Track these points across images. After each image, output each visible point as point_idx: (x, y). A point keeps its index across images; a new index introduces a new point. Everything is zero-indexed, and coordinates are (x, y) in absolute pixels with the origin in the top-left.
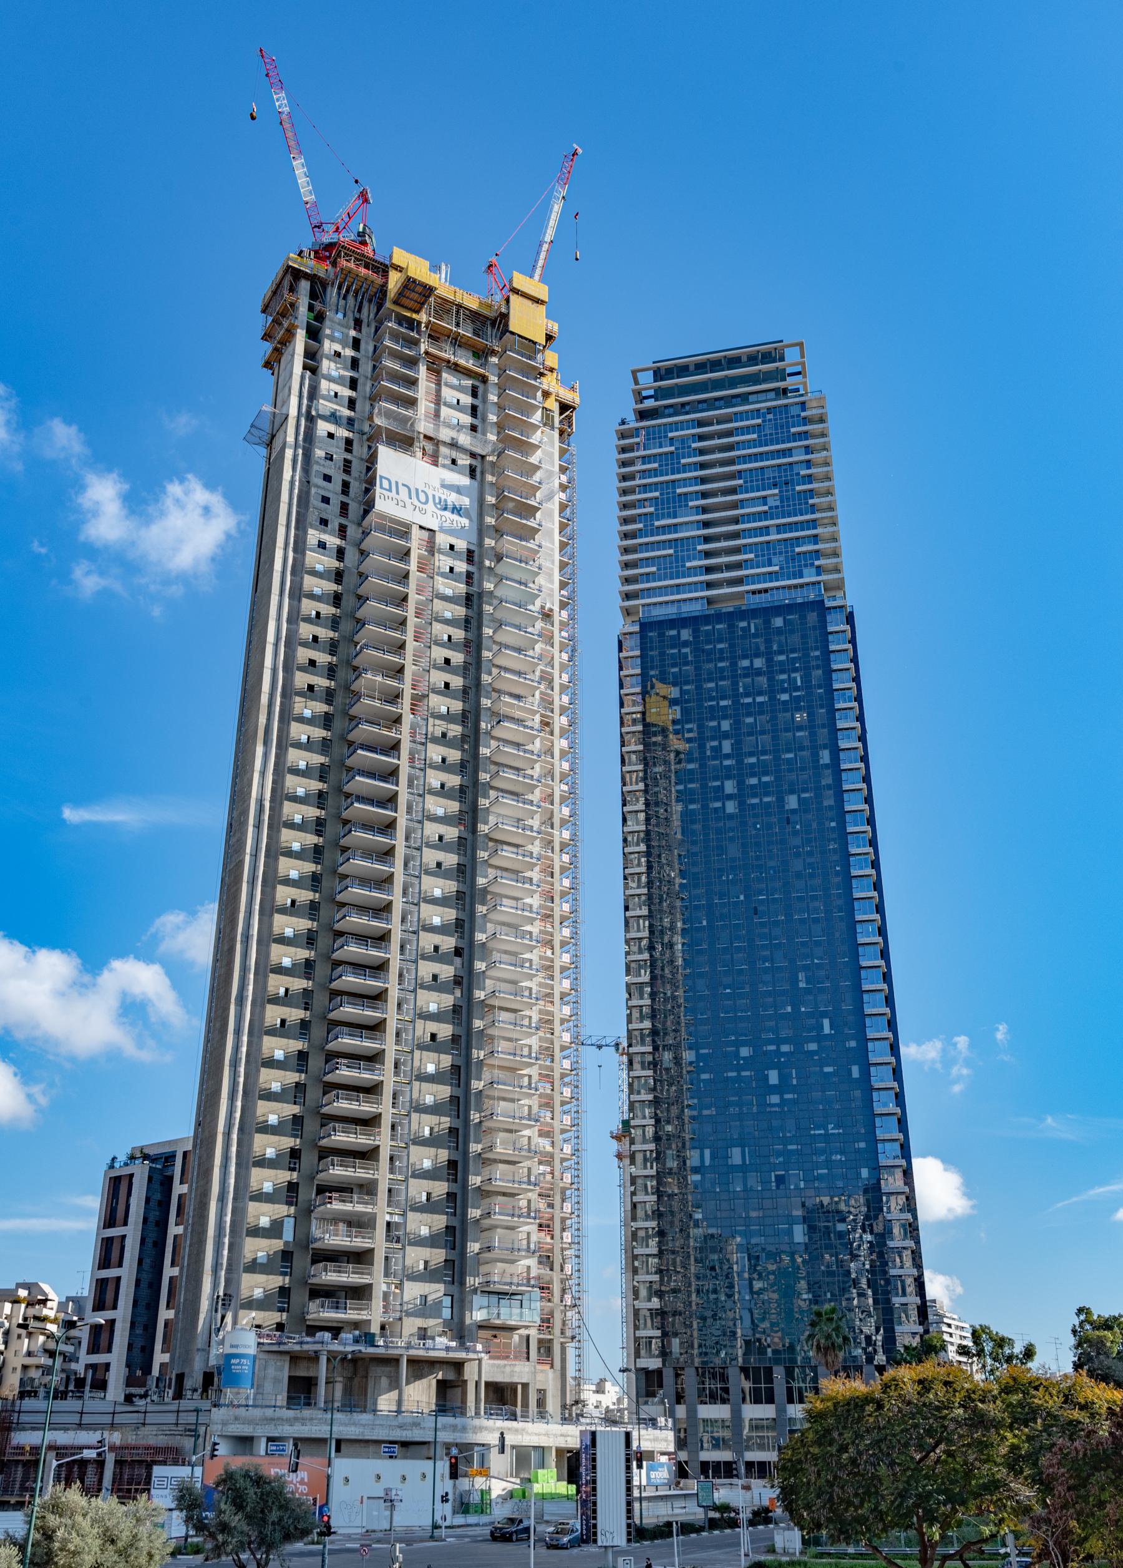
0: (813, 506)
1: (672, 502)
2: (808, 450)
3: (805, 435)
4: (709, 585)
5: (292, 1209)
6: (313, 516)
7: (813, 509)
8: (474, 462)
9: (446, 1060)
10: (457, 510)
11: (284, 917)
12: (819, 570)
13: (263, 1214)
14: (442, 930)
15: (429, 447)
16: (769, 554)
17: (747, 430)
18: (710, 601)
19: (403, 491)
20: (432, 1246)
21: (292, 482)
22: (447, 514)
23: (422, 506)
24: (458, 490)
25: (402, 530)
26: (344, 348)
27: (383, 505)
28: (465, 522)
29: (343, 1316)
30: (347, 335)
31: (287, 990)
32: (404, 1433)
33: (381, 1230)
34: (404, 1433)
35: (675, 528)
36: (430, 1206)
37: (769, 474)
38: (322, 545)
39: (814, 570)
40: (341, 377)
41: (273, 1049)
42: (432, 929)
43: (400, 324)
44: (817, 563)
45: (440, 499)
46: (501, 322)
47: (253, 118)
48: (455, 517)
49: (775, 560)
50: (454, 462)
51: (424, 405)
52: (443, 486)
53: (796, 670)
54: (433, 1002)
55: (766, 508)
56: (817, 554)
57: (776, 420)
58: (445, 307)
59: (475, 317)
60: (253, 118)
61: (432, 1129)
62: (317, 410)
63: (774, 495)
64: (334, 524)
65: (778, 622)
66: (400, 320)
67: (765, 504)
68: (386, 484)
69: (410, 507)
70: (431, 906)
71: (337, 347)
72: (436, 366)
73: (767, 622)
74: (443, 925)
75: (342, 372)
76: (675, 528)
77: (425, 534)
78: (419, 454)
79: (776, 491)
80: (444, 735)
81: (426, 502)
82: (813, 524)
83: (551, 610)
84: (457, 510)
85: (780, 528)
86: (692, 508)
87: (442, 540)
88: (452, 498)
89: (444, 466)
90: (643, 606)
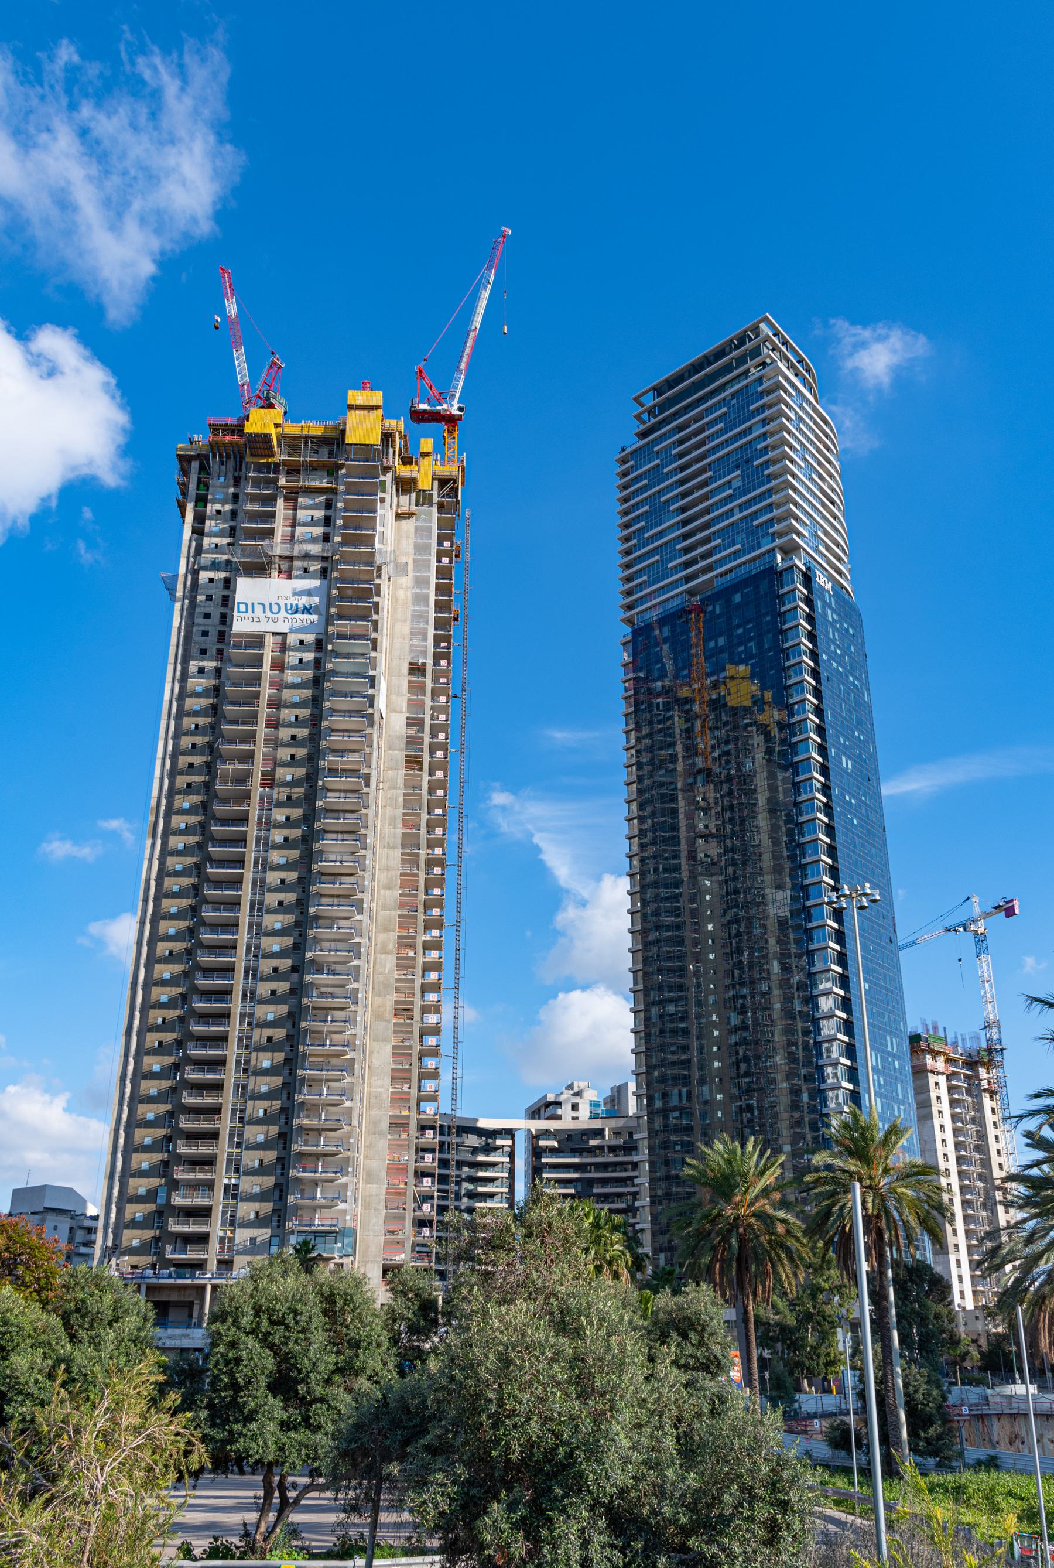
0: (768, 476)
1: (658, 511)
2: (764, 422)
3: (761, 409)
4: (688, 579)
5: (163, 1181)
6: (195, 650)
7: (769, 478)
8: (325, 565)
9: (280, 1057)
10: (306, 610)
11: (162, 966)
12: (774, 536)
13: (140, 1186)
14: (281, 955)
15: (285, 566)
16: (733, 535)
17: (715, 422)
18: (691, 593)
19: (259, 609)
20: (261, 1201)
21: (179, 628)
22: (298, 616)
23: (274, 616)
24: (309, 593)
25: (257, 641)
26: (223, 506)
27: (240, 625)
28: (315, 617)
29: (184, 1256)
30: (227, 493)
31: (164, 1019)
32: (173, 1342)
33: (219, 1192)
34: (173, 1342)
35: (660, 534)
36: (262, 1170)
37: (734, 458)
38: (201, 670)
39: (769, 538)
40: (222, 530)
41: (151, 1065)
42: (272, 955)
43: (260, 472)
44: (771, 531)
45: (291, 605)
46: (335, 441)
47: (217, 328)
48: (306, 616)
49: (738, 539)
50: (306, 570)
51: (281, 529)
52: (295, 594)
53: (750, 639)
54: (269, 1012)
55: (730, 491)
56: (771, 522)
57: (738, 403)
58: (292, 443)
59: (322, 441)
60: (217, 328)
61: (266, 1111)
62: (199, 564)
63: (737, 476)
64: (213, 651)
65: (737, 598)
66: (259, 468)
67: (730, 488)
68: (243, 608)
69: (263, 620)
70: (271, 938)
71: (218, 507)
72: (292, 496)
73: (728, 601)
74: (281, 951)
75: (221, 526)
76: (660, 534)
77: (279, 638)
78: (275, 573)
79: (738, 472)
80: (289, 798)
81: (279, 610)
82: (769, 493)
83: (424, 664)
84: (306, 610)
85: (742, 507)
86: (673, 511)
87: (292, 639)
88: (303, 601)
89: (297, 577)
90: (638, 614)
